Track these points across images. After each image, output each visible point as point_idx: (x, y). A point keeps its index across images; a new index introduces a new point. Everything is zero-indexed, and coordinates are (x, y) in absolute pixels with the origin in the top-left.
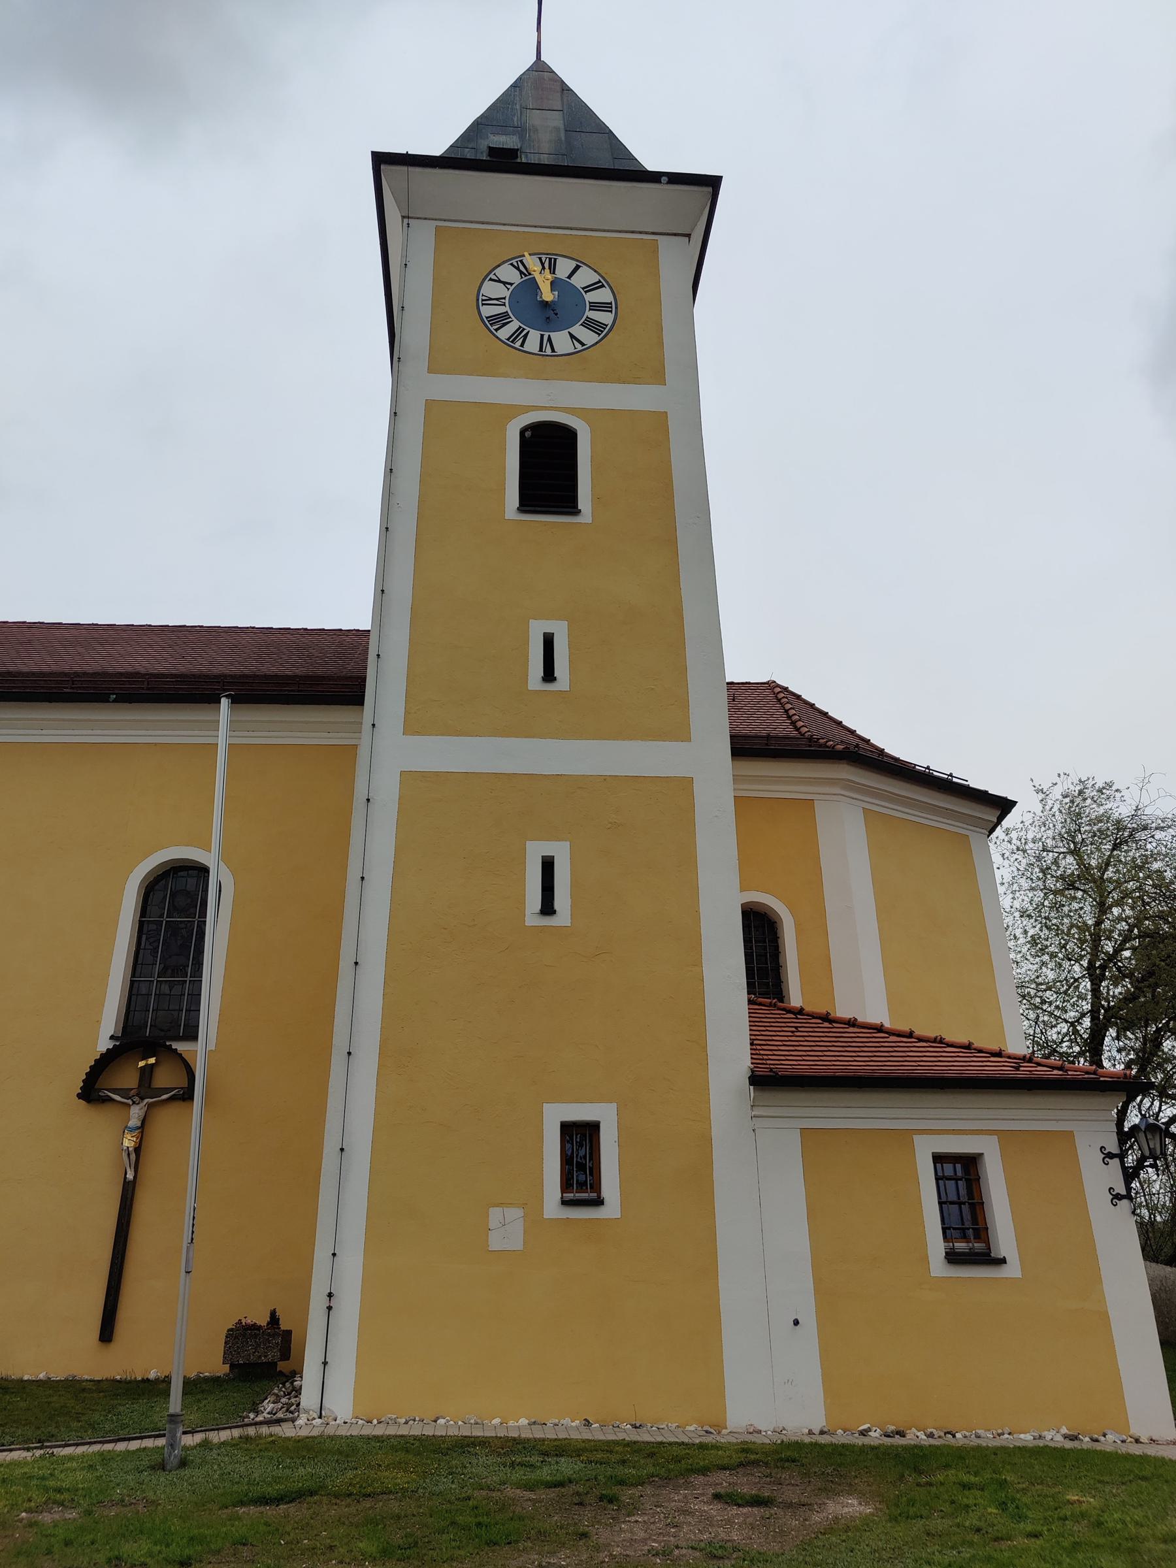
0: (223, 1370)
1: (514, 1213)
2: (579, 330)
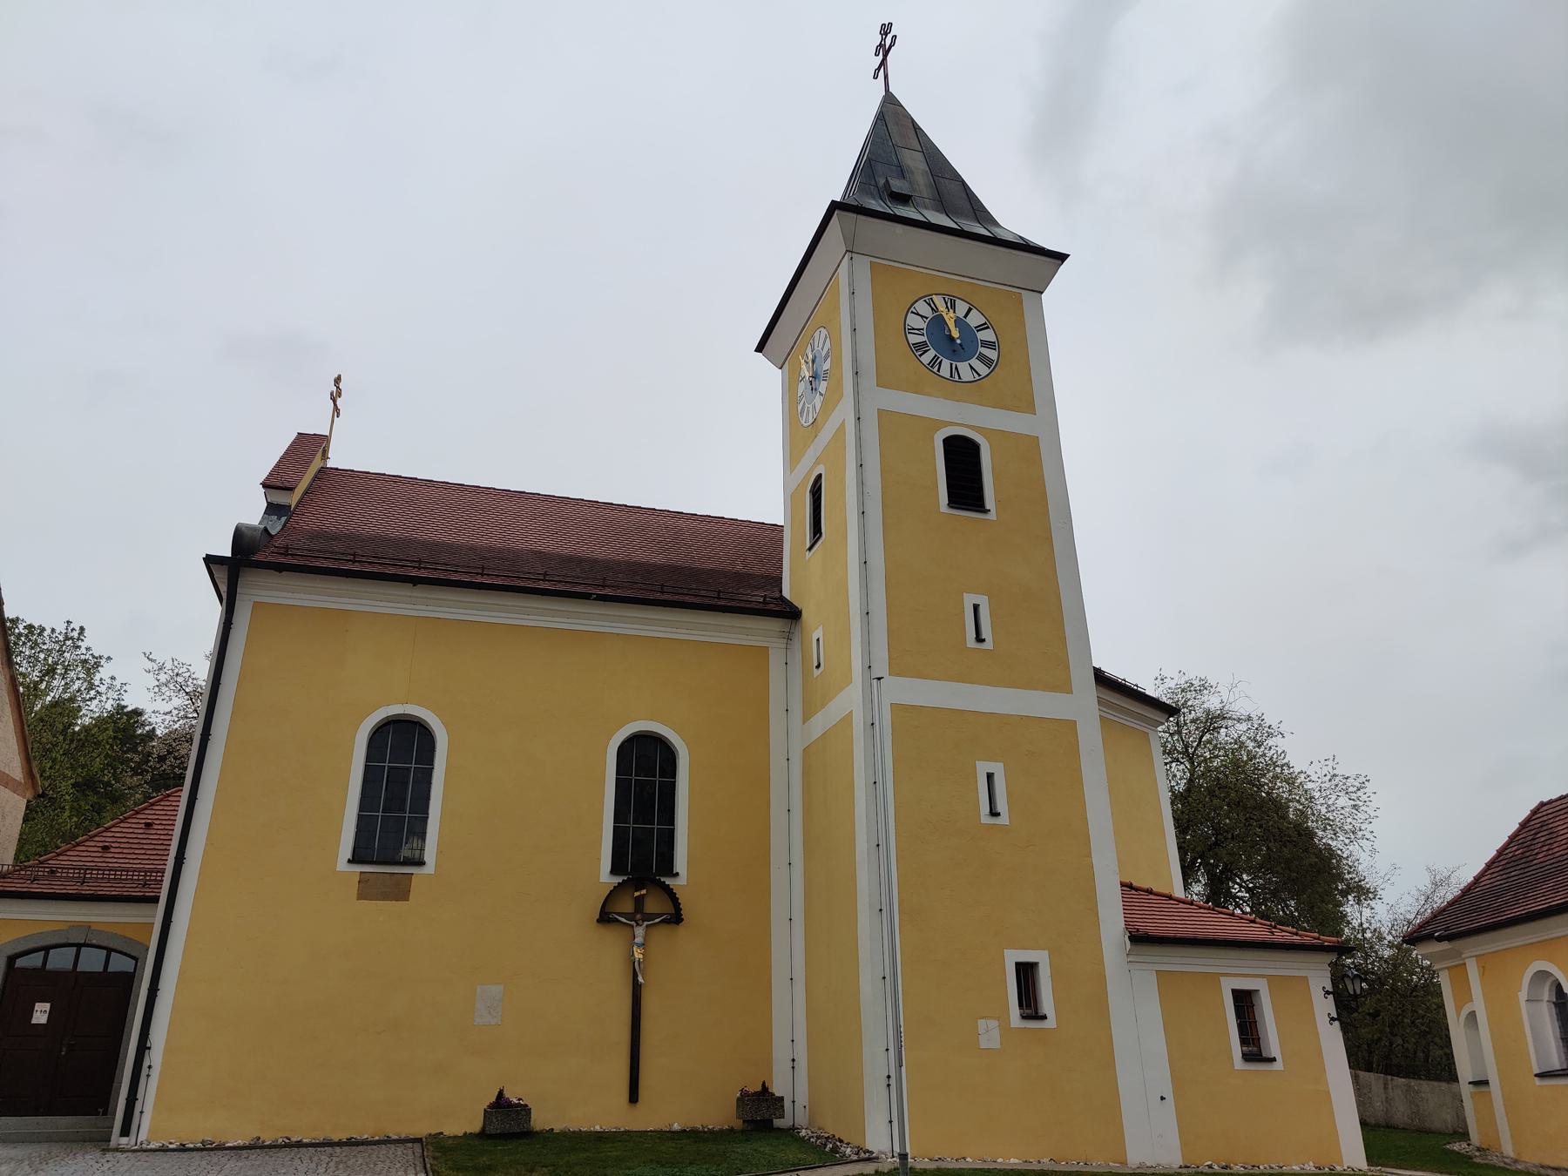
0: (738, 1124)
1: (993, 1024)
2: (975, 362)
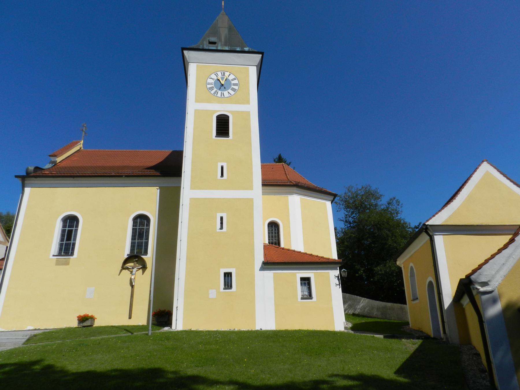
2: (230, 91)
